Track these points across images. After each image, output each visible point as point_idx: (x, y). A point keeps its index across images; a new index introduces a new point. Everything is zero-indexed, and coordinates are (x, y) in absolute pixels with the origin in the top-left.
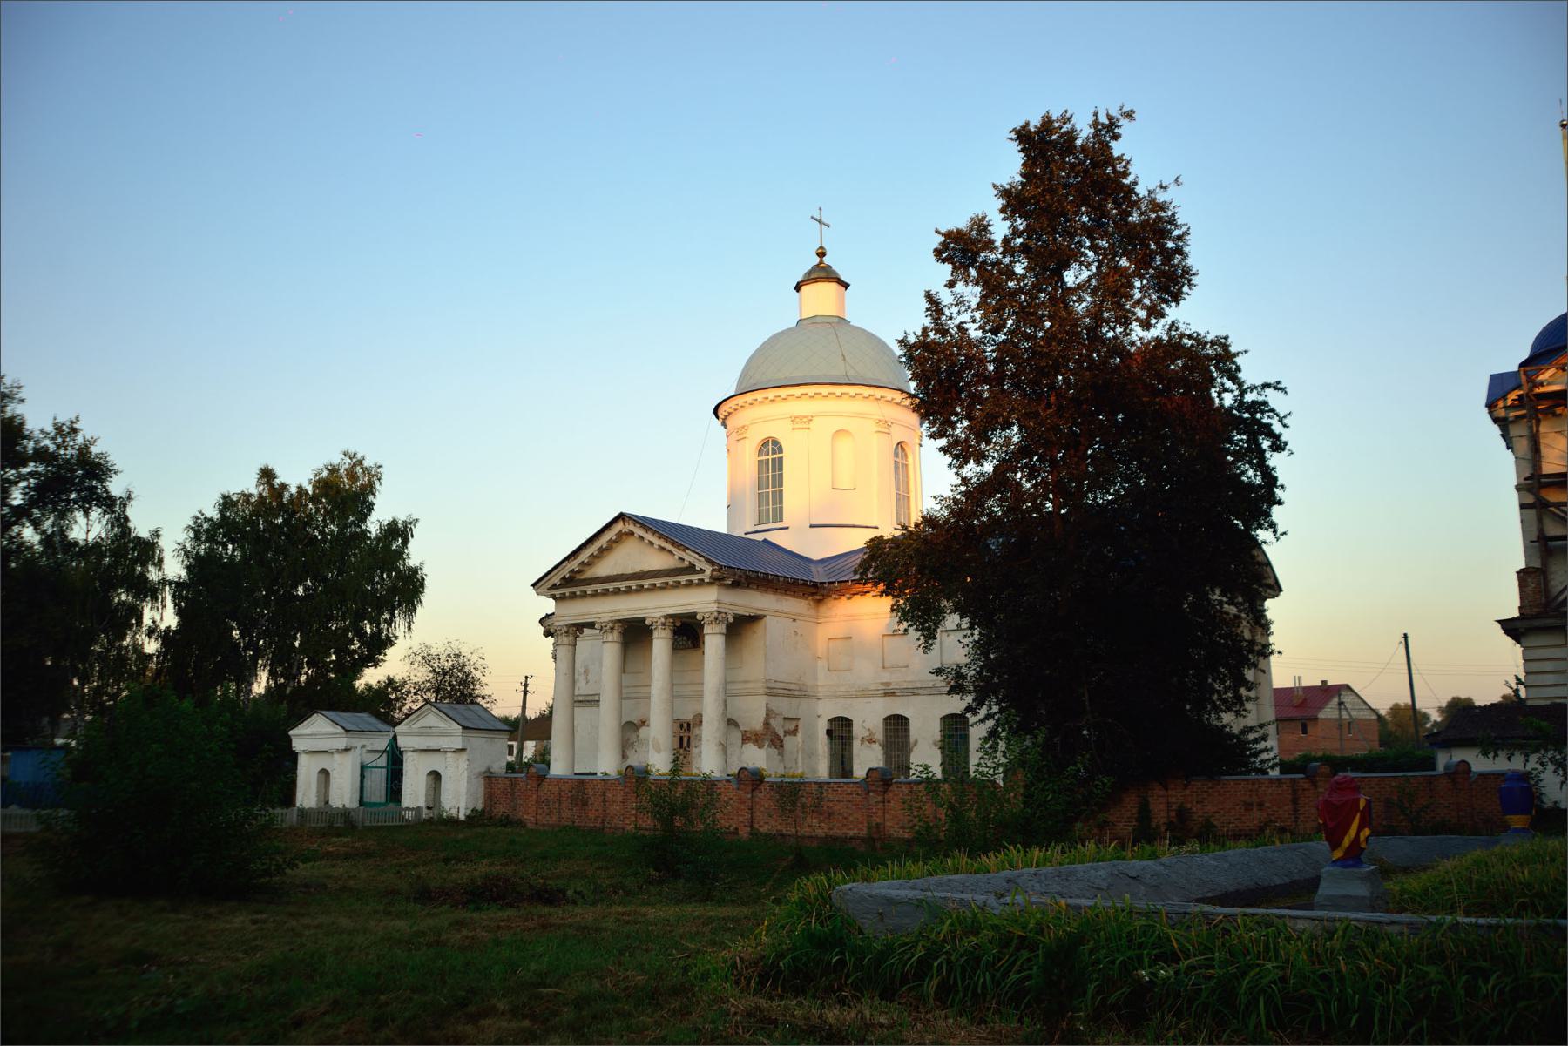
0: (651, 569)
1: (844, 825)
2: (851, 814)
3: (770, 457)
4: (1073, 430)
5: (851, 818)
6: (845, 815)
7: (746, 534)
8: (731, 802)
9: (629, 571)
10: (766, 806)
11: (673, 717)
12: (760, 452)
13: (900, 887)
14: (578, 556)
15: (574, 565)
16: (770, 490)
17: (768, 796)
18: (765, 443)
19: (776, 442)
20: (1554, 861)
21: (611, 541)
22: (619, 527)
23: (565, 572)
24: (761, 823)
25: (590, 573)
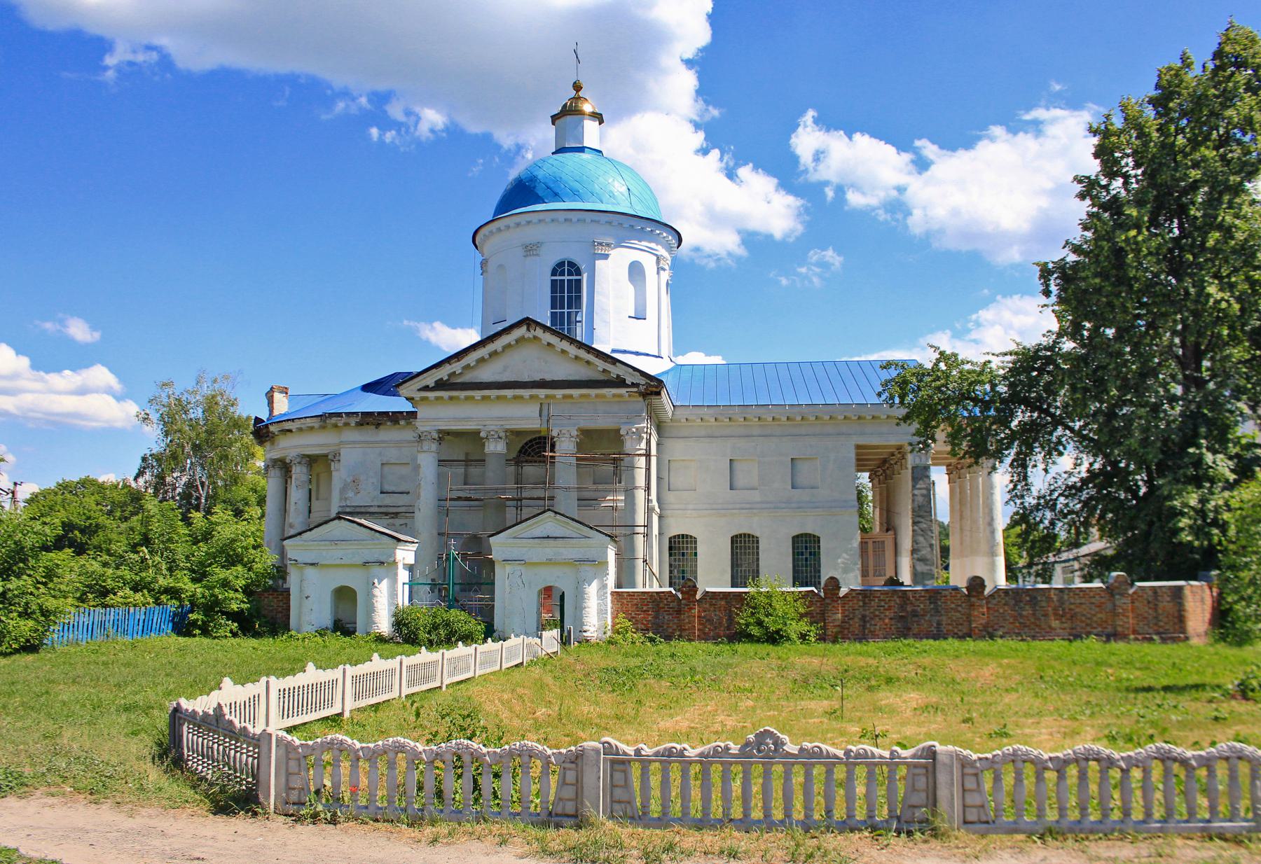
0: (556, 379)
1: (1087, 625)
2: (1094, 615)
3: (566, 278)
4: (1178, 281)
5: (1095, 619)
6: (1089, 616)
7: (614, 351)
8: (960, 609)
9: (527, 379)
10: (1001, 611)
11: (895, 534)
12: (554, 273)
13: (601, 612)
14: (463, 358)
15: (457, 367)
16: (566, 310)
17: (1003, 602)
18: (561, 264)
19: (571, 264)
20: (235, 516)
21: (509, 346)
22: (521, 331)
23: (443, 373)
24: (996, 627)
25: (467, 378)
